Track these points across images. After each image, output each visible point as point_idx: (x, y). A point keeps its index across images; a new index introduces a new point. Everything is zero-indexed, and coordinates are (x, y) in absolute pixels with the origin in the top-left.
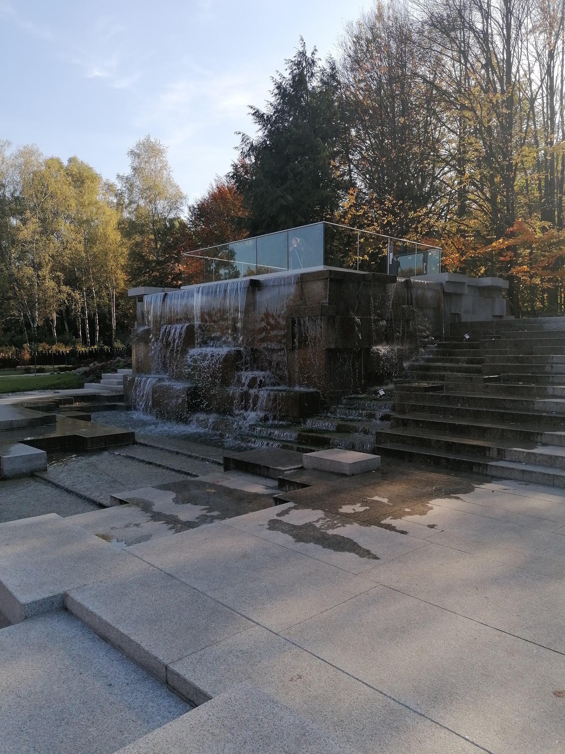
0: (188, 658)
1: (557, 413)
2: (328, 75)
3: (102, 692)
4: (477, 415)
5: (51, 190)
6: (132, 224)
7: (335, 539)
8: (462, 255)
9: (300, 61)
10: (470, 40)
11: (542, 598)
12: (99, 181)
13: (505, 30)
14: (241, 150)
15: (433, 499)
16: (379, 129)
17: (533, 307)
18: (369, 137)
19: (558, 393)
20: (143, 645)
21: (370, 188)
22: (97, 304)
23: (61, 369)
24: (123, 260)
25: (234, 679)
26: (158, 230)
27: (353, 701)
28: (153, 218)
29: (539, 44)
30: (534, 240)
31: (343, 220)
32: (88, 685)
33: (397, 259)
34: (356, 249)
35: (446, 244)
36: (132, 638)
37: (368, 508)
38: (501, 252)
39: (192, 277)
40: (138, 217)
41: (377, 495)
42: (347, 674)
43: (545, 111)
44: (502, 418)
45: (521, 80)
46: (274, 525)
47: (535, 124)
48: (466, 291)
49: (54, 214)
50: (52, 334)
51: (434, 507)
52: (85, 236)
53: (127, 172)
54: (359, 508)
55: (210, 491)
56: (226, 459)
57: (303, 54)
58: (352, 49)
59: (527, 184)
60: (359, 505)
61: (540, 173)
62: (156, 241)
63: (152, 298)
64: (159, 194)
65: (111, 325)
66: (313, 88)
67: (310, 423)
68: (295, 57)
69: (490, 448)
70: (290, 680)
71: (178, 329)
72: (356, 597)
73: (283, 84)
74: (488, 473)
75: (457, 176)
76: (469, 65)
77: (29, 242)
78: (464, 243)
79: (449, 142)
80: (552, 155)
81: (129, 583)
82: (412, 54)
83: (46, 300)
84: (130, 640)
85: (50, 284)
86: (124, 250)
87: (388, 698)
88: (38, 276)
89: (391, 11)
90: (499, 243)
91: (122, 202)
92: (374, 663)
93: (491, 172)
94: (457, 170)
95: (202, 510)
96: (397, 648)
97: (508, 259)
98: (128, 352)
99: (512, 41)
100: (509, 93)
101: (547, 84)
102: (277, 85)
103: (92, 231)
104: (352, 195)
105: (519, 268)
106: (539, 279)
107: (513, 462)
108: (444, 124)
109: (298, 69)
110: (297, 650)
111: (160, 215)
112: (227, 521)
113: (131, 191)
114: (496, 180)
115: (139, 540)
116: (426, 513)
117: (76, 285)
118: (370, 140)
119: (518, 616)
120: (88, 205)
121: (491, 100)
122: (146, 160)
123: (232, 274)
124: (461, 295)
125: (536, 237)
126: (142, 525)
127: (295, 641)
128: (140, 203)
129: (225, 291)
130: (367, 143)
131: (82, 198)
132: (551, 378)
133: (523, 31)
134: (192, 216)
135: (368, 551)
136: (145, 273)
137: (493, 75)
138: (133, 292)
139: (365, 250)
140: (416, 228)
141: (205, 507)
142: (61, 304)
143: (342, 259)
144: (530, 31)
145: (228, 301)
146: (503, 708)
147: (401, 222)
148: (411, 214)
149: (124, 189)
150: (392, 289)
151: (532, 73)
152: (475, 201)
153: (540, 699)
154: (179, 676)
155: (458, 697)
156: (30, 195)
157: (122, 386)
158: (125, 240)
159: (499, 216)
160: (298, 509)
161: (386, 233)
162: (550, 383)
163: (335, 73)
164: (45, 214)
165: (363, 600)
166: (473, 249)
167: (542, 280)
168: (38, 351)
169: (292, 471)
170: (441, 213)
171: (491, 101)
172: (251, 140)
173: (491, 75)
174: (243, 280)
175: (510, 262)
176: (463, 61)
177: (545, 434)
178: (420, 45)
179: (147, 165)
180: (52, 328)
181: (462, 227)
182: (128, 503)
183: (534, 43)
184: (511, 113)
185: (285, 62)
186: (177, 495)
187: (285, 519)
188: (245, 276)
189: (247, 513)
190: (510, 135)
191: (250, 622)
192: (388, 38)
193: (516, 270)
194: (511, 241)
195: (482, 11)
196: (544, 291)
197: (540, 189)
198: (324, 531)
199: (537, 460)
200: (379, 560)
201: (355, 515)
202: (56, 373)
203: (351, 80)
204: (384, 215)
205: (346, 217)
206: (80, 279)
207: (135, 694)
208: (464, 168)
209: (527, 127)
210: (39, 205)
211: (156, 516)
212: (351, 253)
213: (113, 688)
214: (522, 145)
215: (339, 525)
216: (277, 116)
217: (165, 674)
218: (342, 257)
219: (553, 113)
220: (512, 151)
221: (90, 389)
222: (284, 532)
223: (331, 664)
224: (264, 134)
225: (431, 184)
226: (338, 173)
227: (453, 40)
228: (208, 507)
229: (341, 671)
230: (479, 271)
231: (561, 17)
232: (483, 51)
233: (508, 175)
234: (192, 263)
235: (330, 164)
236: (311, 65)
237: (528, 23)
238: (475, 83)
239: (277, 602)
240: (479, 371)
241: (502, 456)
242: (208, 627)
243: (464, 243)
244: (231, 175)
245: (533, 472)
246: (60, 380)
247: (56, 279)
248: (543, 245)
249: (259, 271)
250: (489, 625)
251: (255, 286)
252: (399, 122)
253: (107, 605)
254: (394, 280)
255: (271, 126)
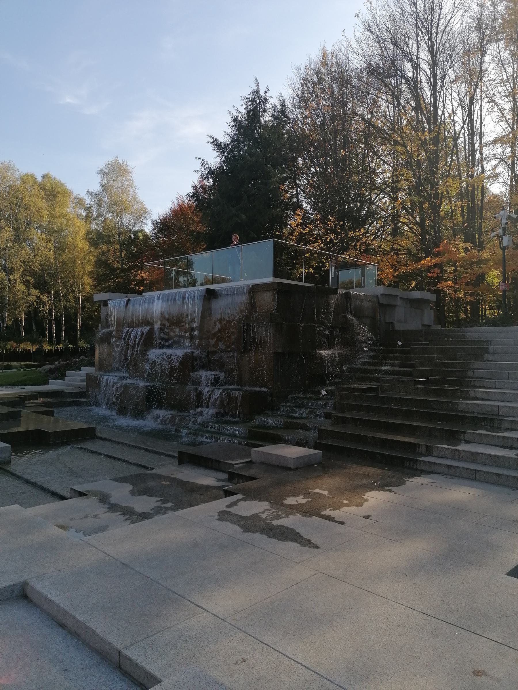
0: (141, 644)
1: (478, 413)
2: (279, 111)
3: (57, 678)
4: (408, 415)
5: (25, 202)
6: (99, 235)
7: (279, 529)
8: (395, 270)
9: (254, 99)
10: (402, 86)
11: (464, 584)
12: (70, 196)
13: (432, 80)
14: (201, 174)
15: (368, 491)
16: (323, 160)
17: (457, 317)
18: (314, 165)
19: (479, 395)
20: (98, 631)
21: (315, 209)
22: (64, 306)
23: (27, 366)
24: (90, 267)
25: (183, 663)
26: (123, 241)
27: (292, 683)
28: (119, 230)
29: (461, 92)
30: (458, 259)
31: (290, 237)
32: (45, 671)
33: (338, 273)
34: (302, 262)
35: (382, 260)
36: (88, 625)
37: (310, 500)
38: (429, 269)
39: (154, 284)
40: (104, 229)
41: (318, 487)
42: (287, 657)
43: (467, 147)
44: (430, 417)
45: (446, 121)
46: (223, 516)
47: (458, 159)
48: (399, 302)
49: (27, 224)
50: (20, 333)
51: (369, 499)
52: (55, 244)
53: (97, 188)
54: (301, 500)
55: (164, 483)
56: (180, 453)
57: (257, 92)
58: (300, 89)
59: (452, 210)
60: (302, 497)
61: (462, 201)
62: (121, 251)
63: (116, 303)
64: (126, 208)
65: (77, 326)
66: (266, 122)
67: (260, 419)
68: (249, 95)
69: (419, 445)
70: (235, 664)
71: (139, 331)
72: (298, 584)
73: (239, 117)
74: (418, 467)
75: (391, 203)
76: (401, 108)
77: (3, 249)
78: (397, 260)
79: (384, 171)
80: (473, 186)
81: (86, 572)
82: (352, 96)
83: (16, 302)
84: (86, 627)
85: (20, 287)
86: (91, 258)
87: (324, 679)
88: (10, 280)
89: (334, 59)
90: (428, 261)
91: (90, 215)
92: (312, 646)
93: (420, 200)
94: (390, 196)
95: (157, 501)
96: (333, 631)
97: (435, 275)
98: (92, 351)
99: (438, 89)
100: (435, 132)
101: (468, 125)
102: (233, 118)
103: (62, 240)
104: (299, 215)
105: (445, 284)
106: (463, 293)
107: (440, 457)
108: (379, 157)
109: (253, 105)
110: (242, 635)
111: (125, 228)
112: (180, 512)
113: (99, 205)
114: (424, 206)
115: (96, 531)
116: (362, 505)
117: (45, 288)
118: (315, 168)
119: (442, 600)
120: (59, 216)
121: (420, 138)
122: (114, 178)
123: (191, 281)
124: (394, 306)
125: (460, 256)
126: (99, 516)
127: (240, 626)
128: (107, 216)
129: (184, 298)
130: (312, 170)
131: (54, 210)
132: (473, 382)
133: (448, 80)
134: (155, 229)
135: (309, 541)
136: (110, 279)
137: (421, 115)
138: (98, 297)
139: (310, 264)
140: (355, 246)
141: (159, 499)
142: (30, 306)
143: (289, 272)
144: (454, 81)
145: (186, 308)
146: (428, 687)
147: (342, 240)
148: (351, 234)
149: (93, 203)
150: (333, 299)
151: (456, 116)
152: (405, 224)
153: (461, 678)
154: (130, 660)
155: (388, 678)
156: (5, 206)
157: (85, 383)
158: (92, 249)
159: (427, 237)
160: (246, 501)
161: (329, 250)
162: (472, 386)
163: (285, 110)
164: (19, 224)
165: (304, 587)
166: (405, 265)
167: (465, 294)
168: (6, 349)
169: (241, 465)
170: (377, 233)
171: (420, 139)
172: (210, 165)
173: (420, 117)
174: (200, 289)
175: (438, 277)
176: (396, 103)
177: (468, 432)
178: (359, 89)
179: (115, 182)
180: (21, 328)
181: (395, 246)
182: (87, 495)
183: (457, 91)
184: (437, 150)
185: (240, 98)
186: (133, 488)
187: (232, 510)
188: (202, 284)
189: (198, 504)
190: (437, 168)
191: (199, 608)
192: (332, 82)
193: (442, 285)
194: (438, 260)
195: (412, 62)
196: (467, 303)
197: (462, 215)
198: (269, 521)
199: (461, 456)
200: (319, 549)
201: (298, 507)
202: (22, 370)
203: (299, 116)
204: (327, 234)
205: (293, 235)
206: (49, 283)
207: (89, 679)
208: (396, 195)
209: (451, 161)
210: (13, 216)
211: (114, 508)
212: (298, 266)
213: (69, 673)
214: (447, 177)
215: (283, 516)
216: (233, 145)
217: (118, 660)
218: (290, 269)
219: (474, 151)
220: (438, 182)
221: (54, 385)
222: (232, 522)
223: (272, 648)
224: (221, 160)
225: (369, 208)
226: (287, 195)
227: (387, 85)
228: (162, 498)
229: (282, 654)
230: (411, 284)
231: (479, 71)
232: (413, 95)
233: (434, 203)
234: (154, 271)
235: (279, 188)
236: (264, 102)
237: (451, 74)
238: (407, 123)
239: (225, 590)
240: (410, 374)
241: (430, 452)
242: (160, 613)
243: (397, 260)
244: (191, 194)
245: (457, 467)
246: (26, 377)
247: (27, 283)
248: (465, 264)
249: (215, 281)
250: (416, 609)
251: (211, 295)
252: (340, 154)
253: (64, 593)
254: (335, 291)
255: (228, 153)
